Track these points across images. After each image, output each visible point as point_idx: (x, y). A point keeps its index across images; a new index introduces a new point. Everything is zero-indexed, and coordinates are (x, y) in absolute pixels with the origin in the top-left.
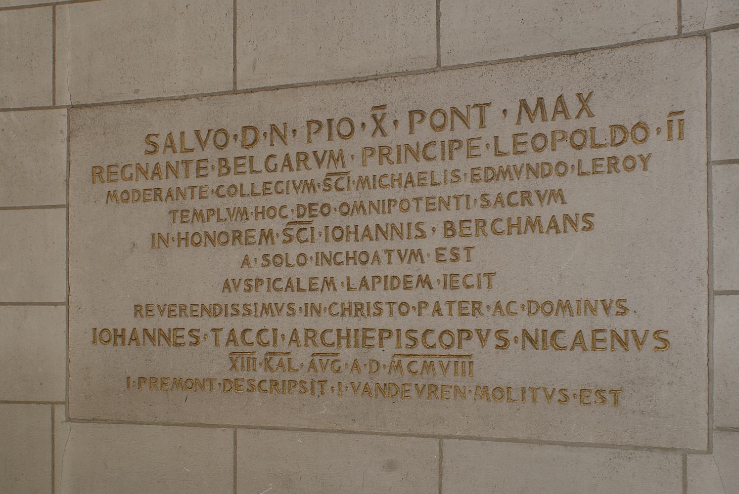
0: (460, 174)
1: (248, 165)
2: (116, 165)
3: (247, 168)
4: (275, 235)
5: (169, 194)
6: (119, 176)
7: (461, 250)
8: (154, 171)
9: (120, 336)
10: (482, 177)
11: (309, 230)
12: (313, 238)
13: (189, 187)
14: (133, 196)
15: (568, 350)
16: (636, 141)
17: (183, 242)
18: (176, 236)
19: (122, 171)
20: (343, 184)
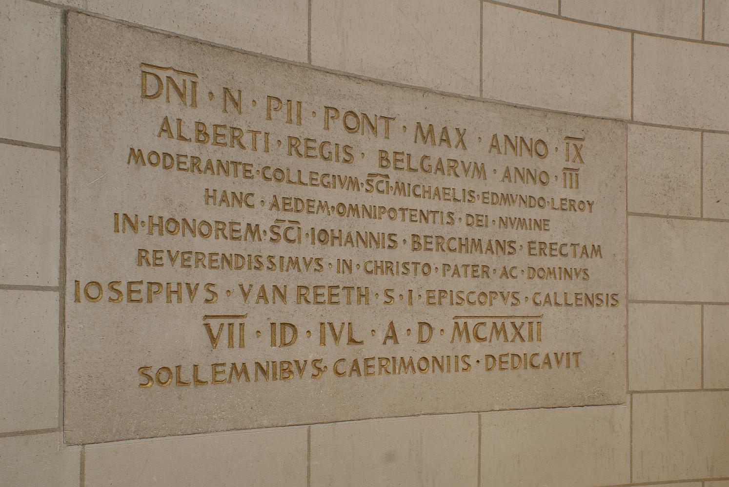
0: (475, 195)
1: (405, 161)
2: (314, 141)
3: (404, 165)
4: (261, 233)
5: (209, 166)
6: (316, 153)
7: (410, 265)
8: (437, 166)
9: (176, 292)
10: (490, 200)
11: (296, 229)
12: (300, 239)
13: (232, 162)
14: (164, 159)
15: (347, 377)
16: (279, 108)
17: (156, 229)
18: (146, 220)
19: (322, 147)
20: (382, 187)
